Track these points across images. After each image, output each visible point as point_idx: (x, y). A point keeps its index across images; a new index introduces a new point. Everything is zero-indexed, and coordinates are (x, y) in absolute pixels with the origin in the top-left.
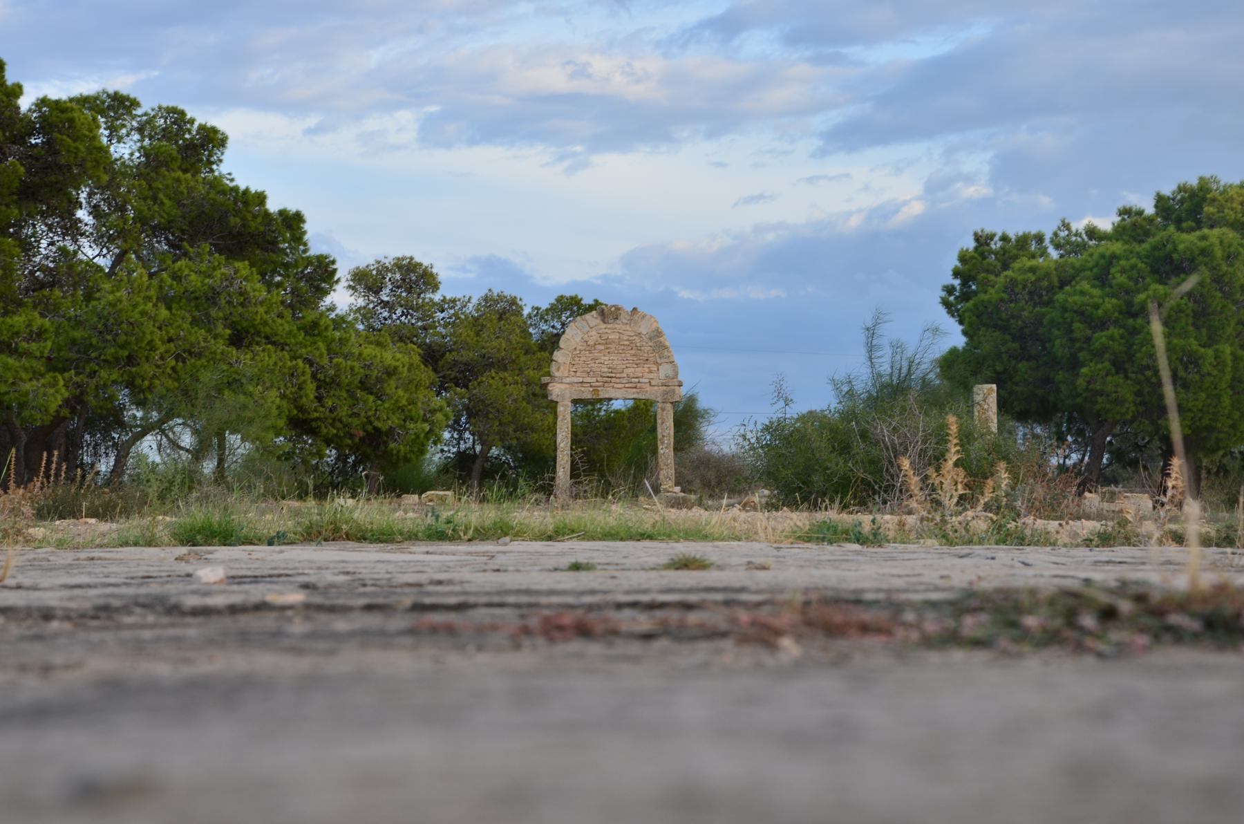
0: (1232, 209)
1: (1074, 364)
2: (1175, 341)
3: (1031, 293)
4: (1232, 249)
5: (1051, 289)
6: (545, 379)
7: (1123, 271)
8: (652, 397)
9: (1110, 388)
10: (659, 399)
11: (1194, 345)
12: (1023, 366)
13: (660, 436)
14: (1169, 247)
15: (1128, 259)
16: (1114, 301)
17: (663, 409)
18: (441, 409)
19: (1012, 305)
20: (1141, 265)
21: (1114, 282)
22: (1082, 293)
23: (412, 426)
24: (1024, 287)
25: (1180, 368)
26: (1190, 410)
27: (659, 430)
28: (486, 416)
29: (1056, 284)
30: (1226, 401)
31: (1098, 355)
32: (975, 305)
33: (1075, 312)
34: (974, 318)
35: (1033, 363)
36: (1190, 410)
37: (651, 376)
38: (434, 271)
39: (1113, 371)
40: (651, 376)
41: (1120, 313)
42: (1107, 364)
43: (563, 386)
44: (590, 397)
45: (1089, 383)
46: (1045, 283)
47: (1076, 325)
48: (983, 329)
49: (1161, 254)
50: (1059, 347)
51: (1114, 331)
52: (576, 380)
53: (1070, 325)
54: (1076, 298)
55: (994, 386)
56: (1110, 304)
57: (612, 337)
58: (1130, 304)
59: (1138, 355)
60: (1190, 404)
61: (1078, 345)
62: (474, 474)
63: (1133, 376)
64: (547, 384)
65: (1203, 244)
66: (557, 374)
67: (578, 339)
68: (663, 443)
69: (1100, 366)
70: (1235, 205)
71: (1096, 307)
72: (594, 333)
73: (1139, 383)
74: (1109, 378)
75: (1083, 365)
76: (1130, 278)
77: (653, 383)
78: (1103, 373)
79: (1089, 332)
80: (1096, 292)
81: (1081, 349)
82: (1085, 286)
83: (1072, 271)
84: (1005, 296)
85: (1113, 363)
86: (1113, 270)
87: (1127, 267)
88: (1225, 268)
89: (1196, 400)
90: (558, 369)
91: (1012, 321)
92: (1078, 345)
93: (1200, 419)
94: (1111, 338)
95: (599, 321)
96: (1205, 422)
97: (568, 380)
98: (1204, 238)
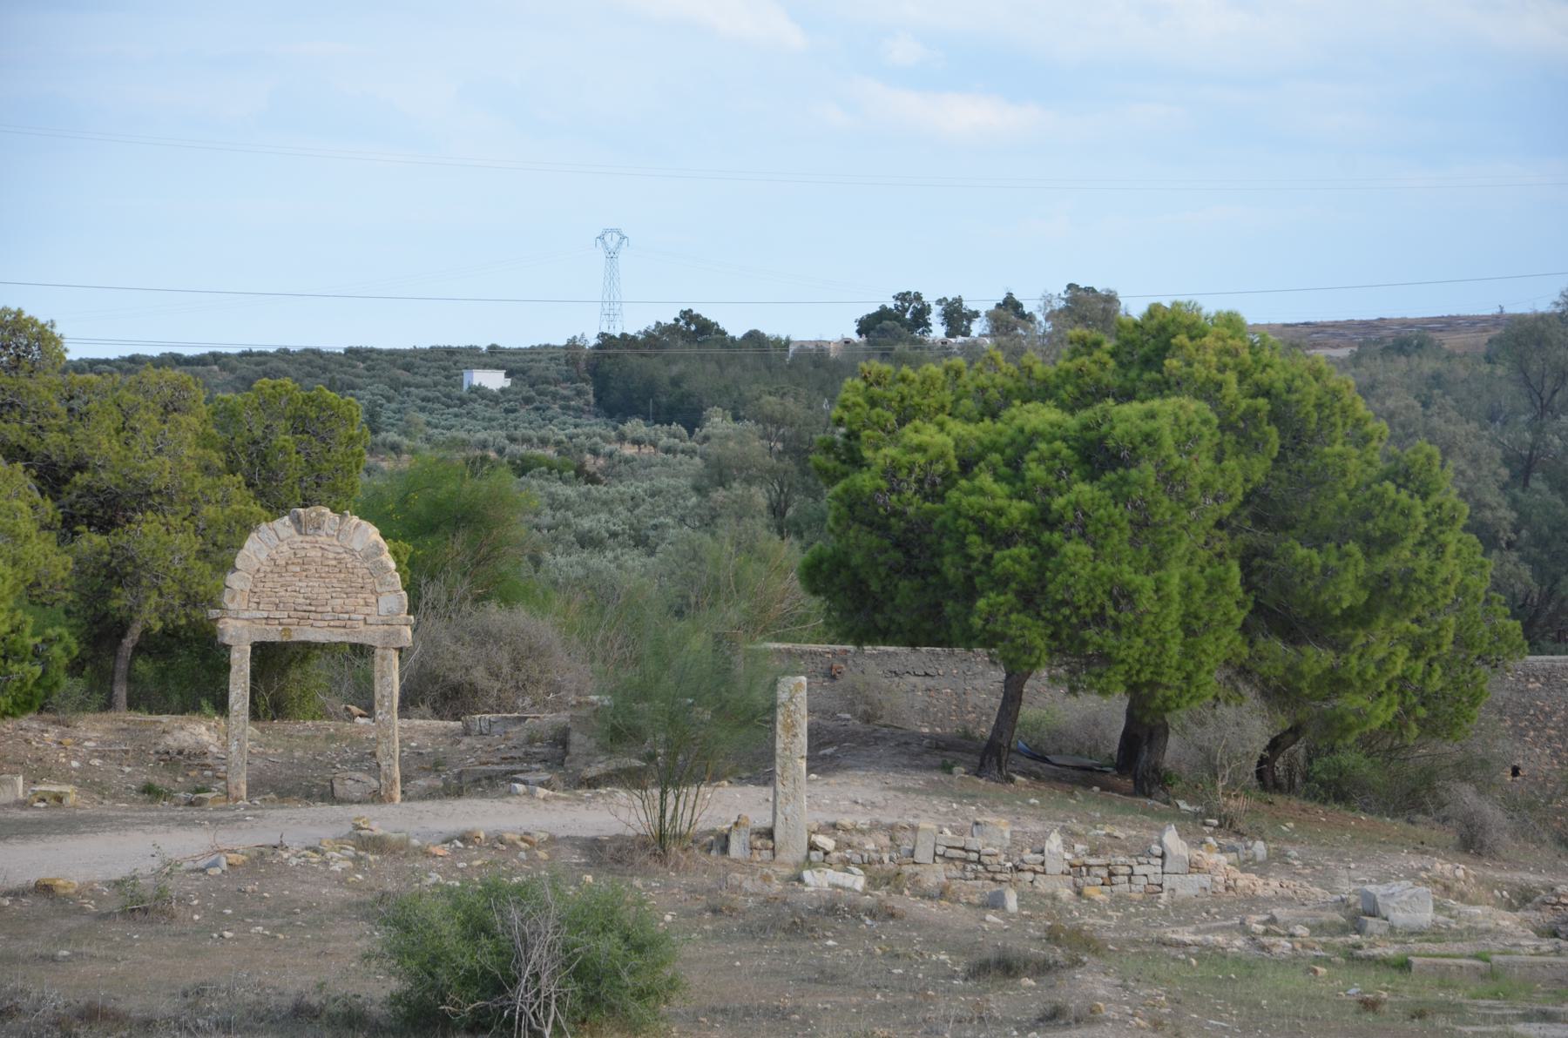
0: (1204, 362)
1: (970, 593)
2: (1102, 568)
3: (920, 481)
4: (1193, 429)
5: (948, 479)
6: (213, 613)
7: (1040, 460)
8: (368, 641)
9: (1013, 632)
10: (377, 644)
11: (1127, 574)
12: (904, 585)
13: (378, 696)
14: (1105, 428)
15: (1050, 442)
16: (1025, 504)
17: (383, 659)
18: (60, 638)
19: (894, 498)
20: (1066, 452)
21: (1029, 475)
22: (982, 492)
23: (16, 668)
24: (911, 471)
25: (1109, 604)
26: (1123, 661)
27: (377, 688)
28: (138, 583)
29: (955, 467)
30: (1174, 648)
31: (1001, 583)
32: (846, 491)
33: (972, 519)
34: (843, 510)
35: (918, 582)
36: (1123, 661)
37: (366, 610)
38: (57, 331)
39: (1019, 606)
40: (366, 610)
41: (1032, 522)
42: (1010, 596)
43: (239, 623)
44: (278, 639)
45: (987, 621)
46: (940, 467)
47: (973, 538)
48: (856, 526)
49: (1092, 435)
50: (950, 567)
51: (1021, 551)
52: (259, 614)
53: (964, 536)
54: (973, 499)
55: (803, 679)
56: (1018, 509)
57: (312, 553)
58: (1046, 509)
59: (1051, 587)
60: (1122, 654)
61: (974, 565)
62: (117, 677)
63: (1047, 615)
64: (217, 620)
65: (1147, 426)
66: (231, 606)
67: (263, 557)
68: (382, 706)
69: (1002, 599)
70: (1208, 357)
71: (1000, 512)
72: (285, 548)
73: (1056, 624)
74: (1013, 617)
75: (981, 594)
76: (1050, 471)
77: (370, 620)
78: (1004, 609)
79: (989, 548)
80: (1001, 489)
81: (979, 572)
82: (986, 480)
83: (978, 449)
84: (883, 484)
85: (1018, 594)
86: (1027, 457)
87: (1047, 454)
88: (1177, 460)
89: (1130, 647)
90: (233, 599)
91: (893, 520)
92: (974, 565)
93: (1138, 672)
94: (1016, 560)
95: (293, 531)
96: (1145, 676)
97: (247, 615)
98: (1152, 415)
